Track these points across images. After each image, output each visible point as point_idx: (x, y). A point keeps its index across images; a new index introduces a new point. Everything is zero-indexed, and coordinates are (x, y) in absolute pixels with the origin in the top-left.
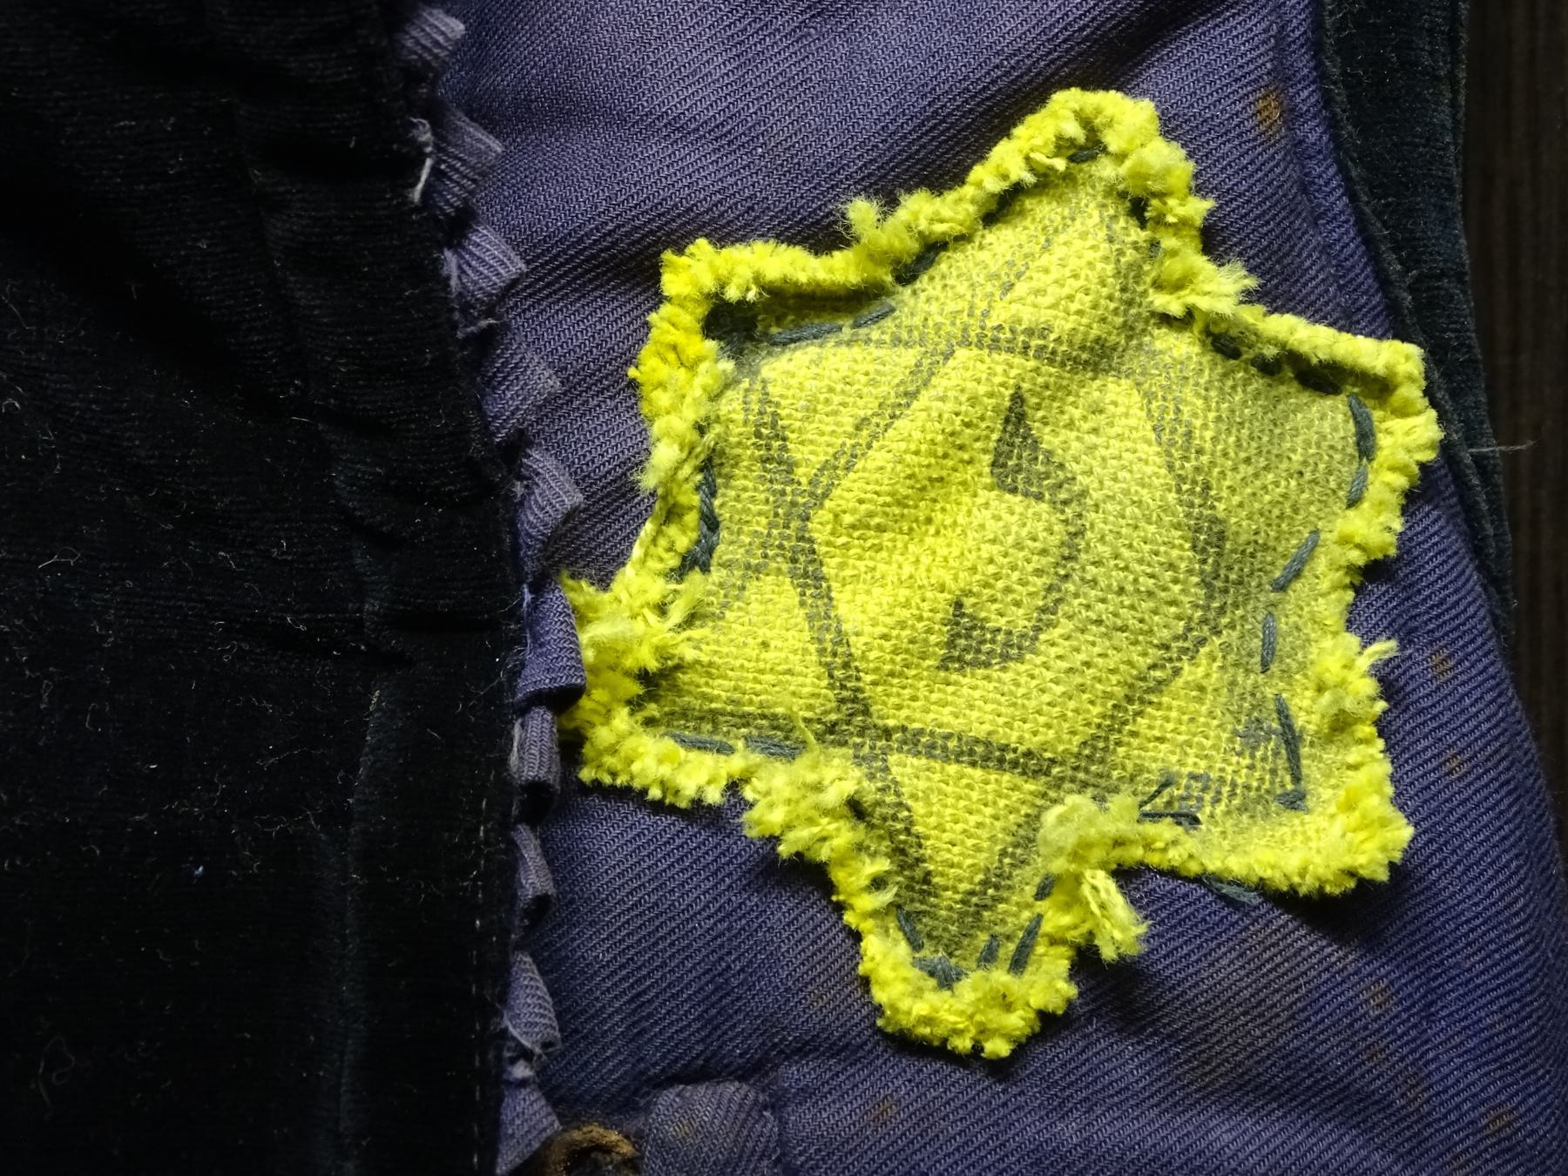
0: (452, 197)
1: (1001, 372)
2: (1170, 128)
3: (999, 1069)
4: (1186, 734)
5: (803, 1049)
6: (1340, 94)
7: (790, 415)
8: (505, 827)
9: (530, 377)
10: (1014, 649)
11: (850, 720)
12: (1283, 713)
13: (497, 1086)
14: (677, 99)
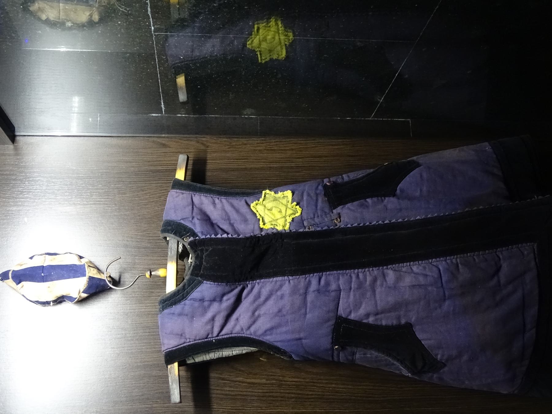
1: (266, 210)
2: (253, 203)
4: (284, 201)
11: (285, 217)
14: (252, 227)
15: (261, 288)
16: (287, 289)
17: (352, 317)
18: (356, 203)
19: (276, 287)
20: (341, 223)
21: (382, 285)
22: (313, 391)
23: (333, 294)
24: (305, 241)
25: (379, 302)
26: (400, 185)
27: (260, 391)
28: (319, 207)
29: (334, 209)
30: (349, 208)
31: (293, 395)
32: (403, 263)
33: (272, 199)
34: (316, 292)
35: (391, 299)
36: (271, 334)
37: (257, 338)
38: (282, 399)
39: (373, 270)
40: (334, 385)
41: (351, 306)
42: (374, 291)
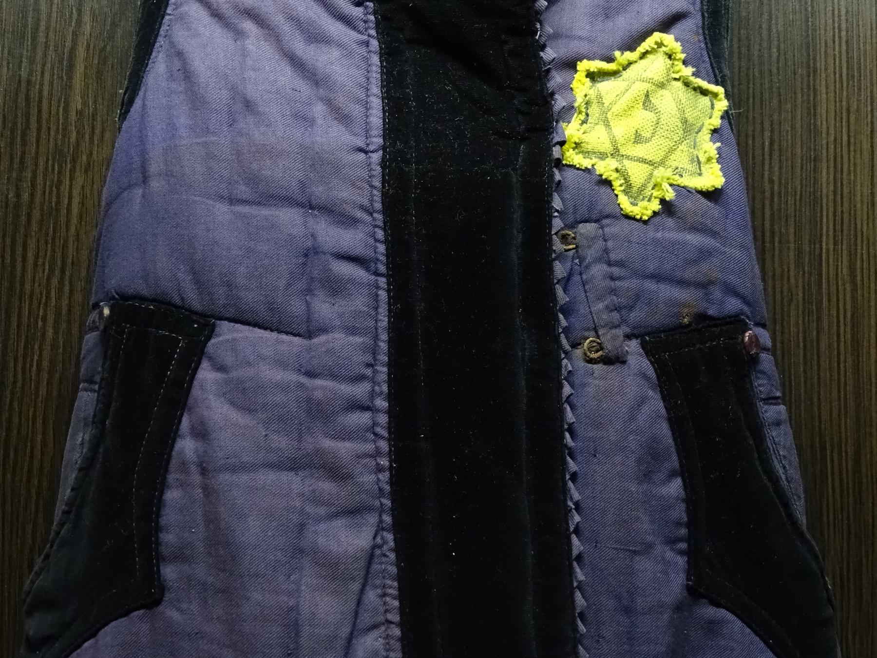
0: (543, 39)
1: (646, 86)
2: (677, 40)
3: (645, 222)
4: (680, 159)
5: (607, 217)
6: (708, 37)
7: (603, 94)
8: (551, 168)
9: (557, 78)
10: (647, 140)
11: (616, 153)
12: (697, 157)
13: (551, 217)
14: (580, 33)
15: (340, 45)
16: (332, 137)
17: (206, 374)
18: (664, 429)
19: (341, 100)
20: (581, 364)
21: (316, 499)
22: (36, 265)
23: (296, 307)
24: (517, 216)
25: (244, 478)
26: (739, 623)
27: (46, 88)
28: (650, 285)
29: (643, 345)
30: (642, 400)
31: (26, 196)
32: (401, 597)
33: (690, 116)
34: (309, 244)
35: (251, 531)
36: (171, 78)
37: (164, 28)
38: (17, 160)
39: (380, 469)
40: (50, 333)
41: (249, 372)
42: (294, 465)
